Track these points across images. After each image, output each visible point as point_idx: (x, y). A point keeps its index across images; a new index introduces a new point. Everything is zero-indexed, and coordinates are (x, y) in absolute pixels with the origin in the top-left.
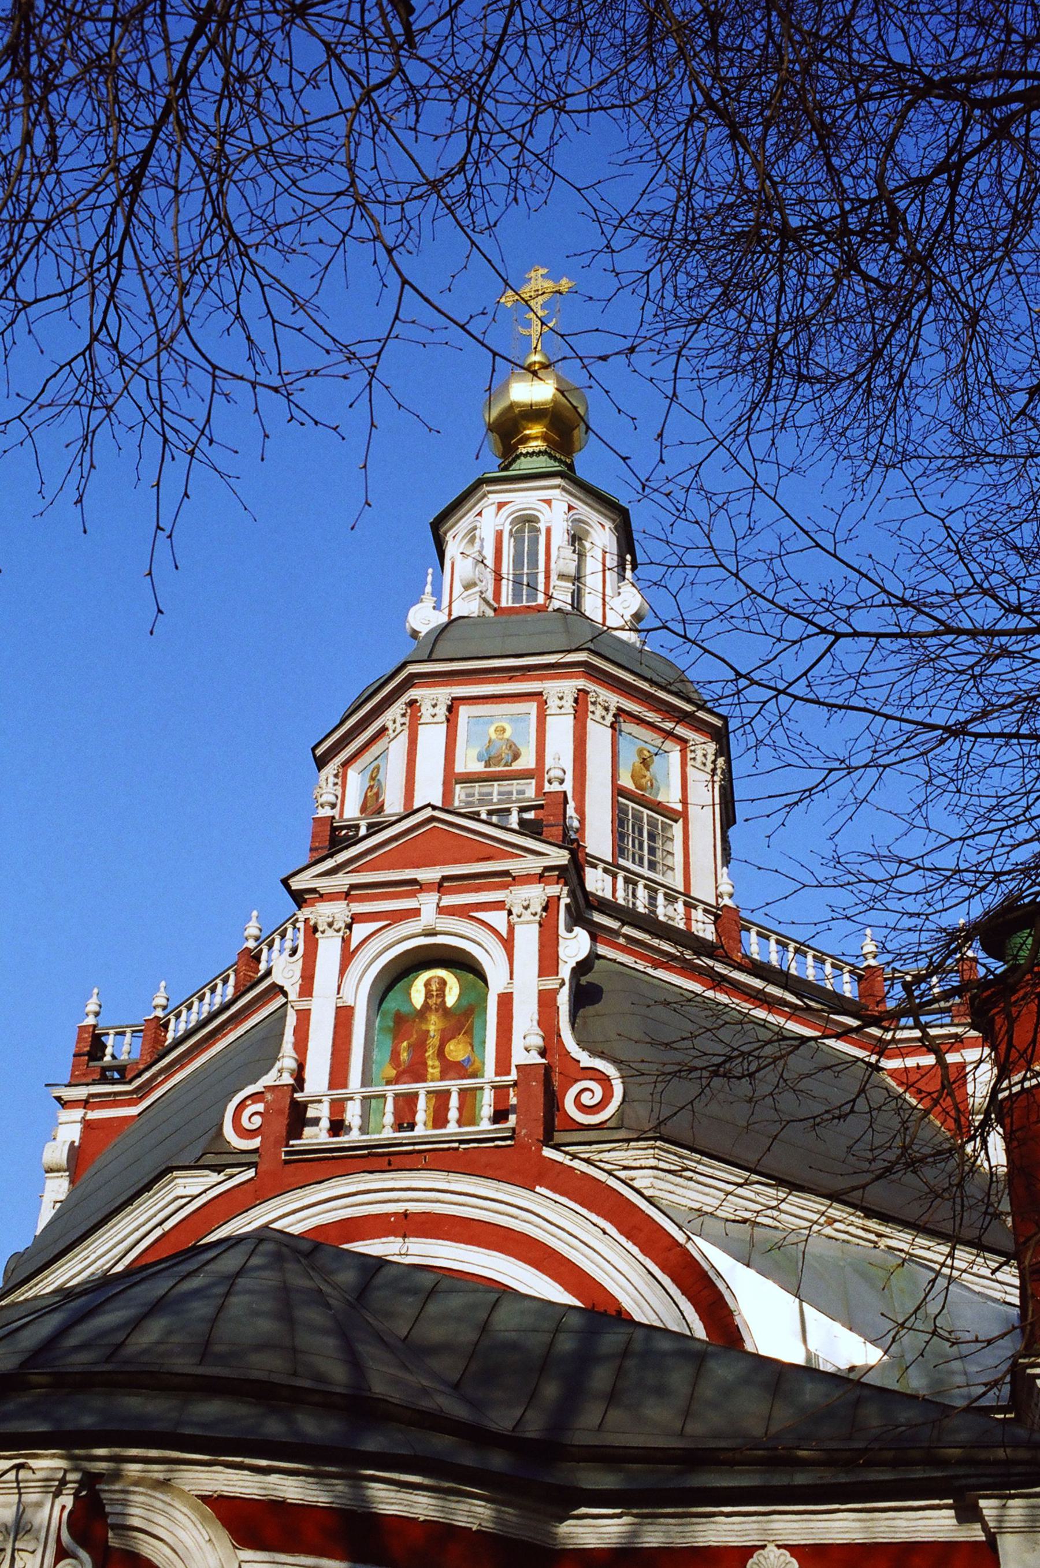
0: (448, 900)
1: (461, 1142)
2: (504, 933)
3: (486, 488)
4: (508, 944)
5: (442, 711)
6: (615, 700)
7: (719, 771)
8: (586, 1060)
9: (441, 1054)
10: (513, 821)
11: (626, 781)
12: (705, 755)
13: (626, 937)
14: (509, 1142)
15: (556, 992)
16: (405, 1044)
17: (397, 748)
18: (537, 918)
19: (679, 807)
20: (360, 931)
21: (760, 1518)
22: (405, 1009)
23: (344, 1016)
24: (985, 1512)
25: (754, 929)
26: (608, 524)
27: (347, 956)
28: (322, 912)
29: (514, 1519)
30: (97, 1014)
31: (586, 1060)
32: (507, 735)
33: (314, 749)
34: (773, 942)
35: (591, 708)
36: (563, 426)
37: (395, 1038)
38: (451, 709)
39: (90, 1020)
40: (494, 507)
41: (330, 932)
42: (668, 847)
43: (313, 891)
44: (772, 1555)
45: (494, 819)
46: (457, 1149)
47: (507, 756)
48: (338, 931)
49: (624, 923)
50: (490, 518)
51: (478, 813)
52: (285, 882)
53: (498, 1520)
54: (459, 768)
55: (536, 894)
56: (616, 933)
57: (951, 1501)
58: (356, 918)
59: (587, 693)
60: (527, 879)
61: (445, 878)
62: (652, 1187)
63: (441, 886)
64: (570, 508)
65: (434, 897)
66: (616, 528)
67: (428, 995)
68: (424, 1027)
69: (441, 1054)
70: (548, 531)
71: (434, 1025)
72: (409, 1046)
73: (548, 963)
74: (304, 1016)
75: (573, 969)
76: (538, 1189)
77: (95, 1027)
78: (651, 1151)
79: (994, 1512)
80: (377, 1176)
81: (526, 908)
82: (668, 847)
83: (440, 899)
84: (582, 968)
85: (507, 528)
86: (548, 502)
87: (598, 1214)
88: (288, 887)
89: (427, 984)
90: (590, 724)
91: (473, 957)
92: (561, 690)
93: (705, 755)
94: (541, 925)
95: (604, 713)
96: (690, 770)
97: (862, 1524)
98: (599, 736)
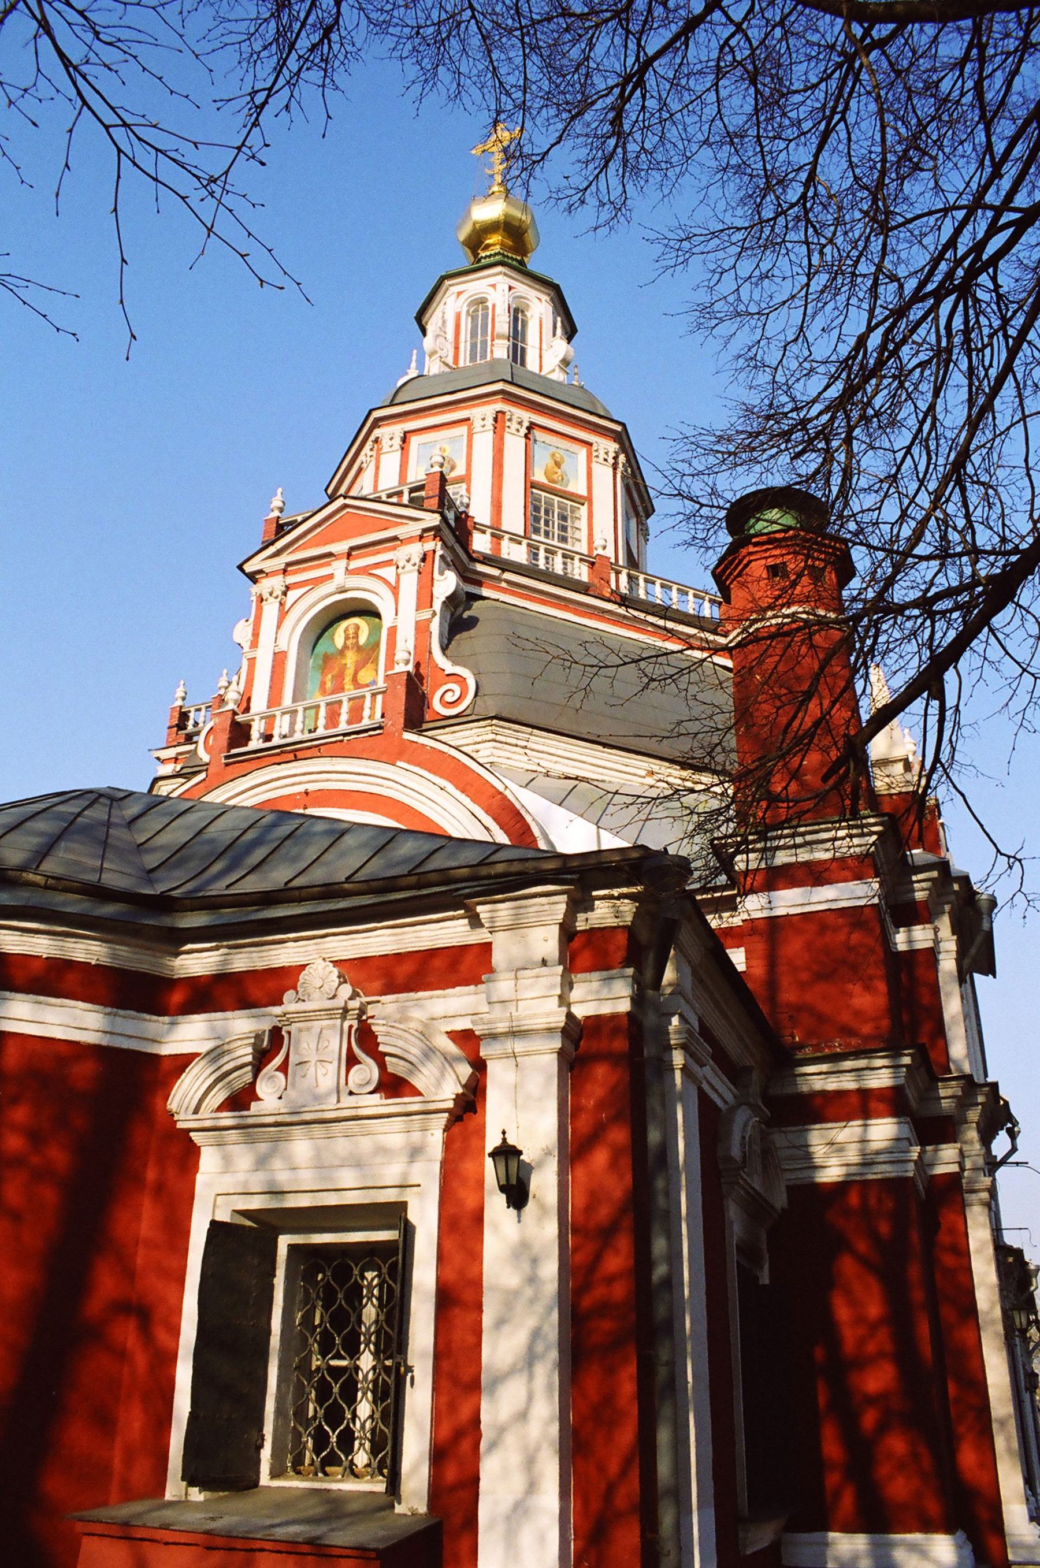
0: (354, 564)
1: (344, 735)
2: (393, 583)
3: (447, 283)
4: (395, 590)
5: (397, 442)
6: (527, 416)
7: (621, 465)
8: (449, 667)
10: (405, 499)
11: (539, 476)
12: (606, 453)
13: (508, 582)
14: (378, 732)
15: (429, 621)
16: (330, 676)
18: (416, 567)
19: (584, 492)
20: (293, 595)
21: (319, 940)
22: (330, 650)
23: (279, 659)
24: (482, 916)
25: (658, 582)
26: (545, 298)
28: (265, 585)
29: (130, 955)
30: (184, 699)
31: (449, 667)
33: (326, 490)
34: (691, 597)
35: (508, 424)
36: (515, 234)
37: (322, 673)
38: (404, 440)
39: (179, 703)
41: (271, 599)
42: (577, 524)
43: (261, 571)
44: (320, 967)
45: (394, 500)
46: (342, 741)
48: (276, 597)
49: (504, 570)
50: (452, 304)
51: (380, 497)
52: (240, 567)
53: (114, 956)
55: (416, 550)
56: (498, 579)
57: (462, 912)
59: (503, 413)
60: (410, 540)
61: (352, 549)
62: (492, 755)
64: (510, 288)
65: (343, 562)
66: (552, 299)
67: (347, 638)
68: (343, 662)
70: (494, 306)
71: (350, 659)
72: (333, 677)
73: (425, 598)
74: (252, 661)
75: (444, 602)
76: (399, 763)
77: (181, 707)
78: (489, 728)
79: (488, 915)
80: (283, 766)
81: (408, 561)
82: (577, 524)
83: (348, 564)
84: (452, 601)
85: (465, 309)
86: (494, 286)
87: (441, 777)
88: (243, 571)
89: (346, 630)
90: (507, 436)
91: (366, 600)
92: (483, 414)
93: (606, 453)
94: (420, 573)
95: (519, 427)
96: (594, 465)
97: (394, 938)
98: (514, 445)
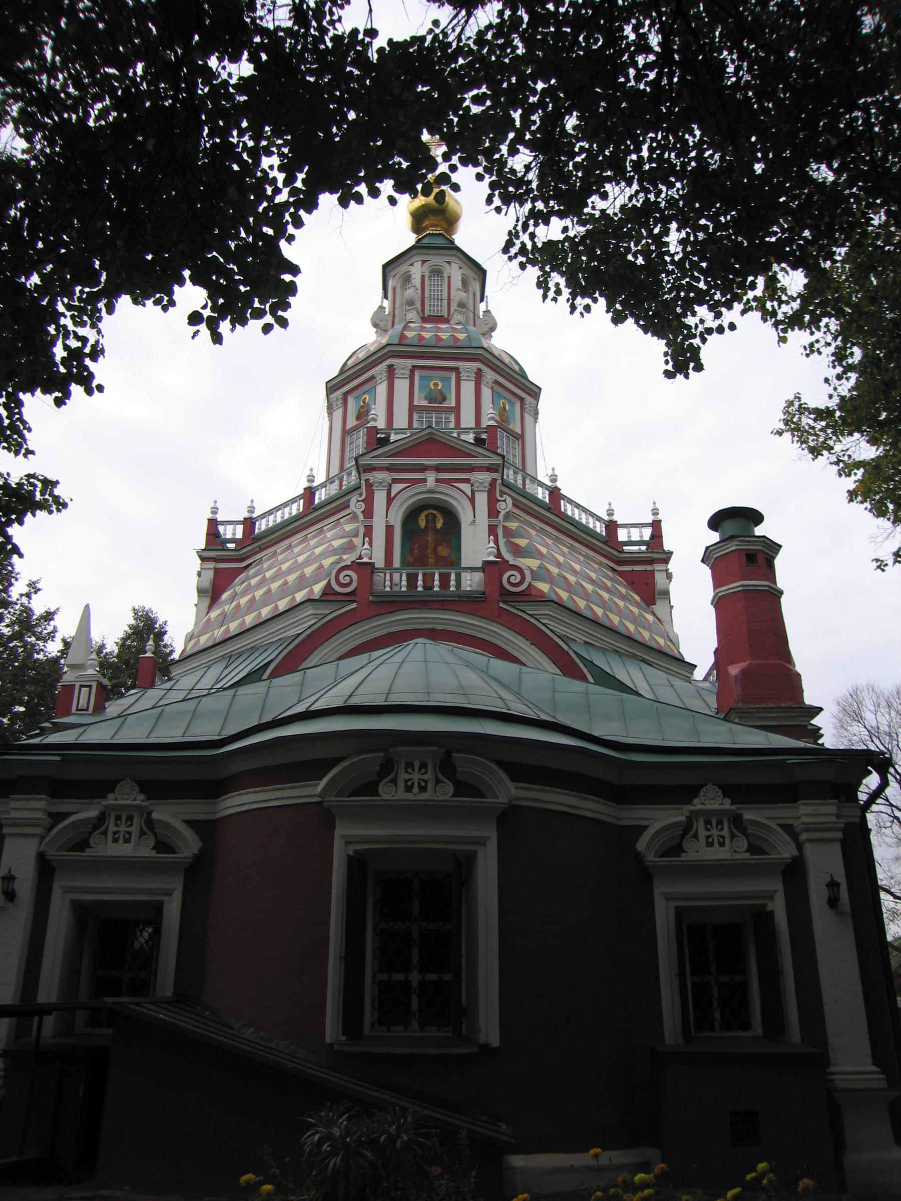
2: (470, 495)
4: (472, 500)
9: (435, 551)
17: (382, 390)
23: (389, 529)
27: (390, 500)
32: (439, 387)
40: (420, 263)
47: (439, 398)
54: (416, 403)
58: (395, 481)
63: (438, 469)
69: (435, 551)
70: (449, 278)
89: (426, 517)
